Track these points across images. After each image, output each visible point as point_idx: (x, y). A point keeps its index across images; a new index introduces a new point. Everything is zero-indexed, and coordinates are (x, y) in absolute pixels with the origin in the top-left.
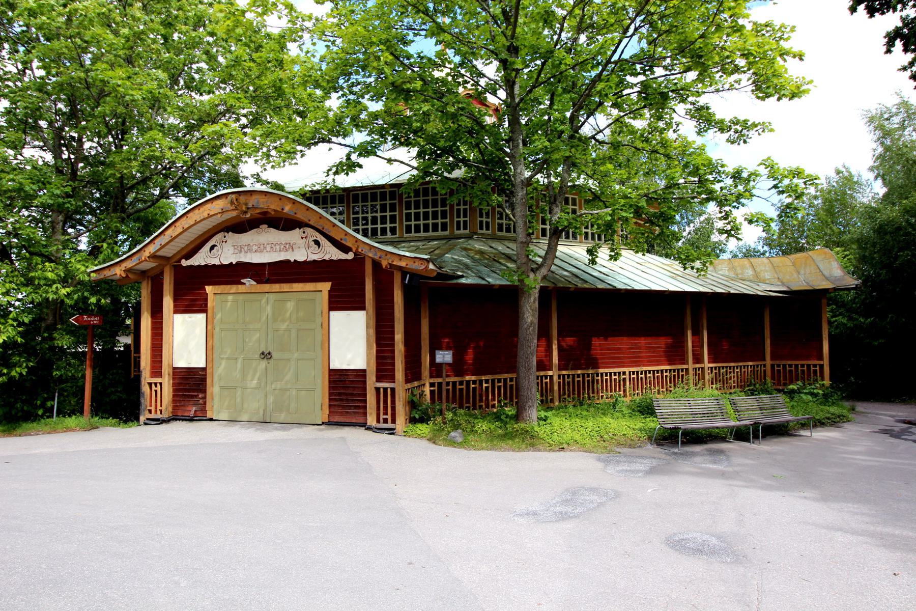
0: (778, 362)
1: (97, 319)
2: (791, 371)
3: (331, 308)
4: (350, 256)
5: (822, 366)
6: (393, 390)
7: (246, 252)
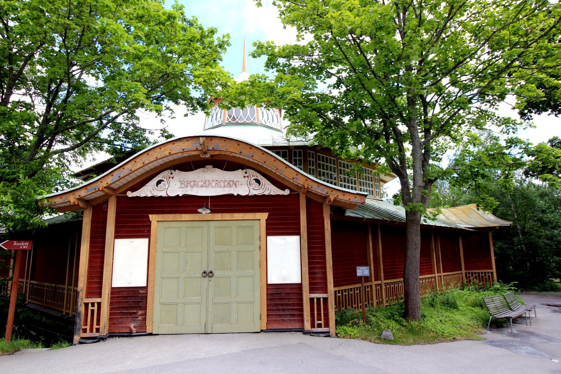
0: (469, 271)
1: (27, 244)
2: (482, 276)
3: (268, 234)
4: (287, 192)
5: (492, 273)
6: (325, 300)
7: (192, 187)
